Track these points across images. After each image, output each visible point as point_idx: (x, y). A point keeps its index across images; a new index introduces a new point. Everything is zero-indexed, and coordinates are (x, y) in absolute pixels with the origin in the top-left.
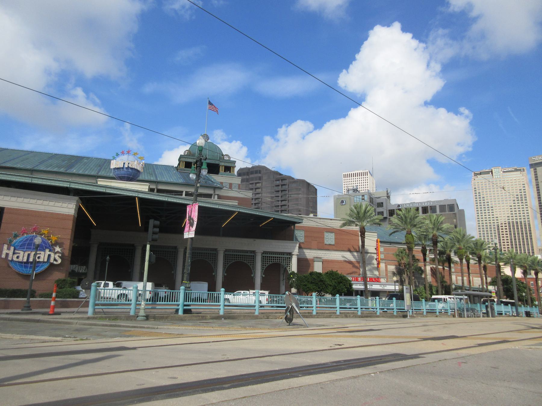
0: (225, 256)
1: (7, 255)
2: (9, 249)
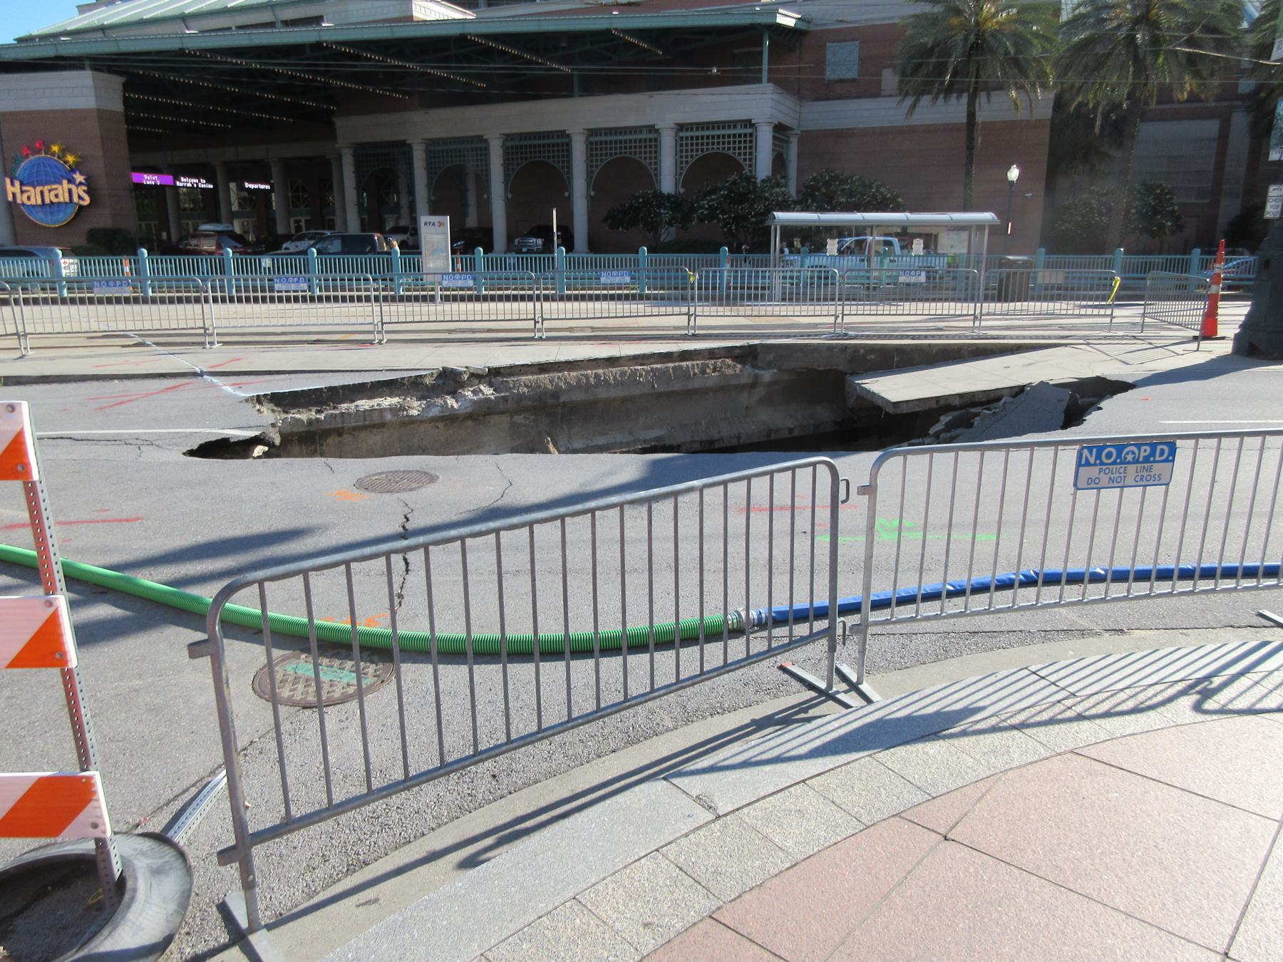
0: (591, 148)
1: (14, 195)
2: (13, 184)
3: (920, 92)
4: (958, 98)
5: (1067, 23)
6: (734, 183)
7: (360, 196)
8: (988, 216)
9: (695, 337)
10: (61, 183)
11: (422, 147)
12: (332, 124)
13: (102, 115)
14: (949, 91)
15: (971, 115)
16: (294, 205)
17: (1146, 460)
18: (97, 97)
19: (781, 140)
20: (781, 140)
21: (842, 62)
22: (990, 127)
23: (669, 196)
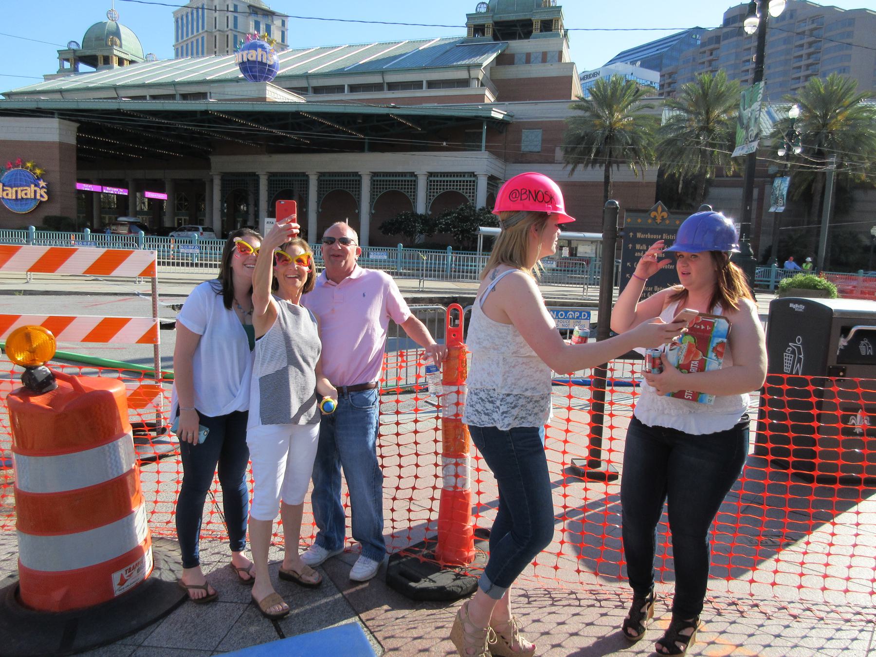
0: (373, 183)
3: (576, 162)
4: (600, 166)
5: (663, 127)
6: (462, 209)
7: (222, 205)
8: (600, 235)
9: (423, 292)
10: (29, 186)
11: (266, 177)
12: (208, 160)
13: (62, 146)
14: (594, 162)
15: (607, 177)
16: (178, 209)
17: (578, 318)
18: (60, 134)
19: (493, 186)
20: (493, 186)
21: (531, 141)
22: (616, 184)
23: (421, 215)
